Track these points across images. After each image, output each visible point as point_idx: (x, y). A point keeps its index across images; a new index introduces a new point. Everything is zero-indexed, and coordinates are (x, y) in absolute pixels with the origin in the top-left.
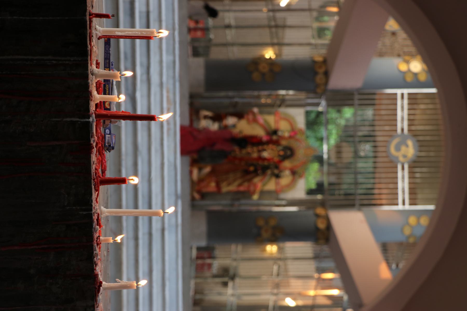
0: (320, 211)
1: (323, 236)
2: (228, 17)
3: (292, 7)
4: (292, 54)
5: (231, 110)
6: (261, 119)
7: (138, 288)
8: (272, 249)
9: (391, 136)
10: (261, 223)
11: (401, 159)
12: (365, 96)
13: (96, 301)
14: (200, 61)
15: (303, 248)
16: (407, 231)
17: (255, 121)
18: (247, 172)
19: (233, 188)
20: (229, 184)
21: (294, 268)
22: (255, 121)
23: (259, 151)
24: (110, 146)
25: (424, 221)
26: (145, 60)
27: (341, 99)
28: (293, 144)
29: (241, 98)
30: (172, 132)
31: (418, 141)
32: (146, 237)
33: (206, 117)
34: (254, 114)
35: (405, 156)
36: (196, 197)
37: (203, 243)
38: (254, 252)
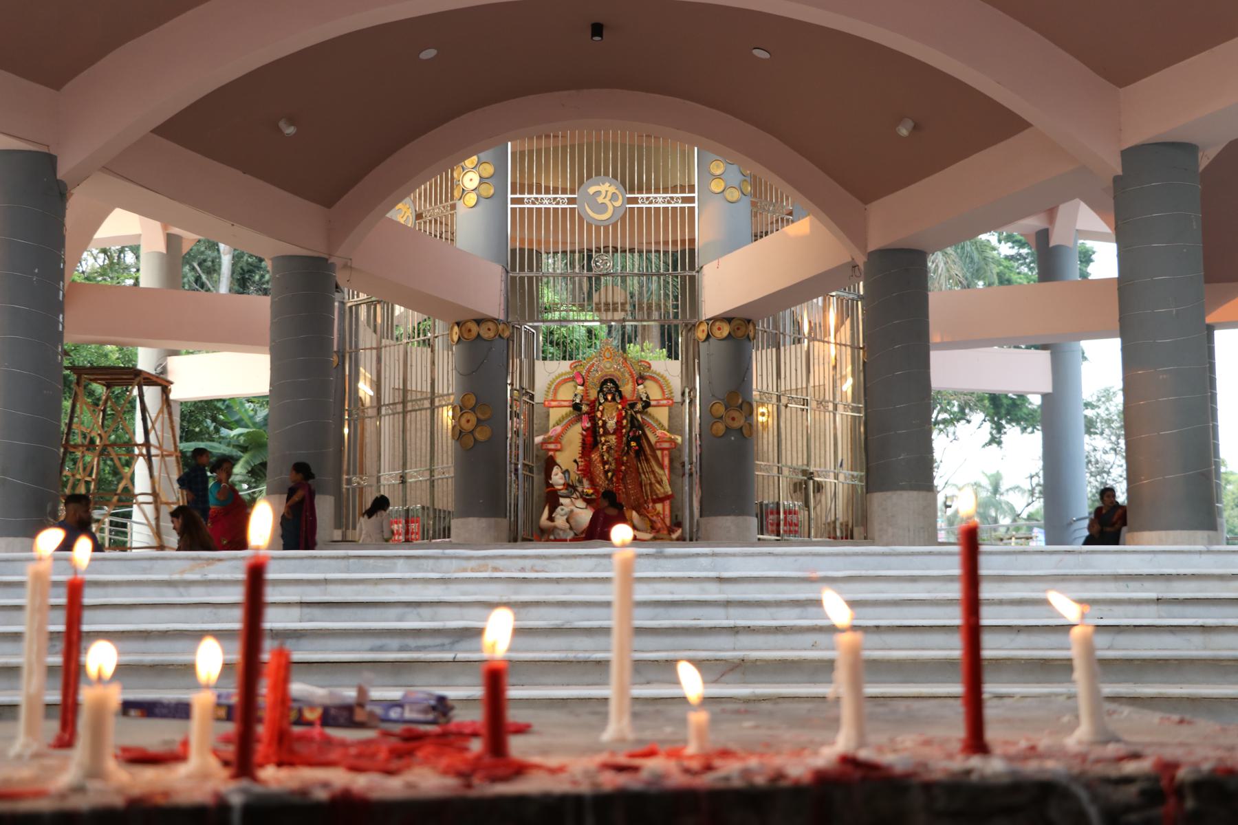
0: (701, 333)
1: (742, 328)
2: (388, 482)
3: (375, 378)
4: (448, 380)
5: (538, 478)
6: (555, 431)
7: (854, 628)
8: (763, 415)
10: (720, 428)
11: (618, 204)
13: (908, 776)
14: (456, 524)
15: (761, 363)
16: (734, 195)
17: (558, 439)
18: (640, 452)
19: (664, 475)
20: (660, 482)
21: (793, 379)
22: (558, 439)
23: (606, 433)
24: (434, 708)
25: (718, 168)
26: (393, 612)
27: (522, 295)
28: (597, 376)
29: (516, 458)
30: (538, 562)
31: (589, 177)
32: (732, 611)
33: (551, 519)
34: (544, 442)
35: (614, 197)
36: (669, 529)
37: (754, 522)
38: (766, 442)
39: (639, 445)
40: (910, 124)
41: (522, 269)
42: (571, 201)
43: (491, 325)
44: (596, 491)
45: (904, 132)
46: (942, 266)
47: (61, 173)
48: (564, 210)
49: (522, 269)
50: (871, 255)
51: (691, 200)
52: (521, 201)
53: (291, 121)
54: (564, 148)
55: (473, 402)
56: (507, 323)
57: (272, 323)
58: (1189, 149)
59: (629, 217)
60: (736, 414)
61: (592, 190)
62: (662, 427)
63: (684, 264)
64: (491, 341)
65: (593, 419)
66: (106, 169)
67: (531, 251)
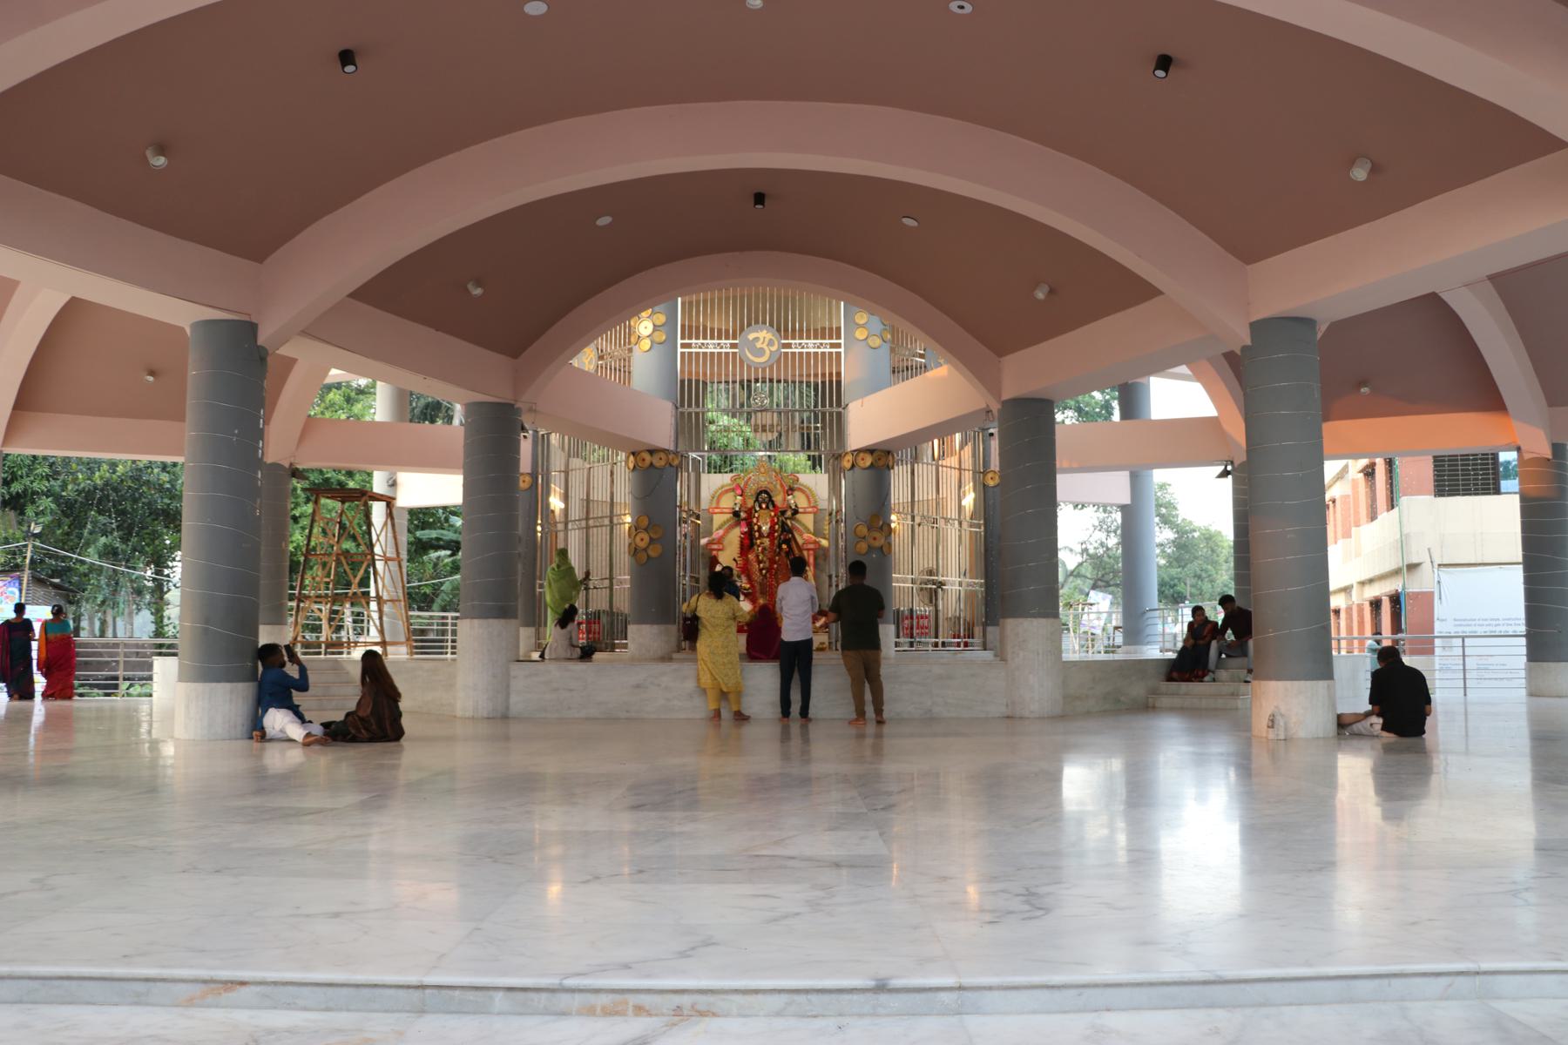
0: (847, 463)
1: (881, 458)
4: (624, 491)
9: (742, 362)
10: (863, 546)
11: (774, 348)
12: (687, 395)
15: (899, 480)
16: (877, 342)
22: (720, 541)
23: (761, 536)
25: (862, 318)
27: (690, 425)
28: (752, 489)
31: (749, 325)
34: (710, 543)
35: (771, 343)
39: (789, 547)
40: (1046, 288)
41: (690, 405)
42: (733, 346)
43: (662, 455)
44: (752, 586)
45: (1040, 295)
46: (1065, 417)
47: (262, 340)
48: (727, 354)
49: (690, 405)
50: (1005, 403)
51: (838, 346)
52: (689, 346)
53: (478, 284)
54: (727, 299)
55: (646, 522)
56: (676, 453)
57: (466, 445)
58: (1308, 323)
59: (783, 359)
60: (877, 534)
61: (751, 336)
62: (808, 531)
63: (828, 398)
64: (661, 469)
65: (750, 525)
66: (305, 333)
67: (697, 381)
